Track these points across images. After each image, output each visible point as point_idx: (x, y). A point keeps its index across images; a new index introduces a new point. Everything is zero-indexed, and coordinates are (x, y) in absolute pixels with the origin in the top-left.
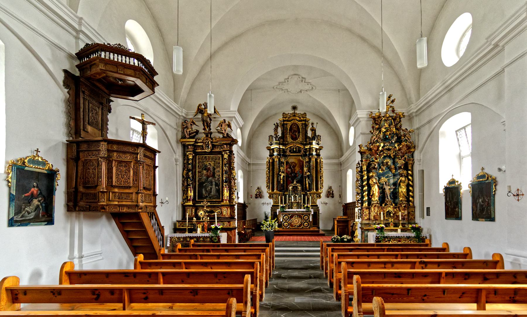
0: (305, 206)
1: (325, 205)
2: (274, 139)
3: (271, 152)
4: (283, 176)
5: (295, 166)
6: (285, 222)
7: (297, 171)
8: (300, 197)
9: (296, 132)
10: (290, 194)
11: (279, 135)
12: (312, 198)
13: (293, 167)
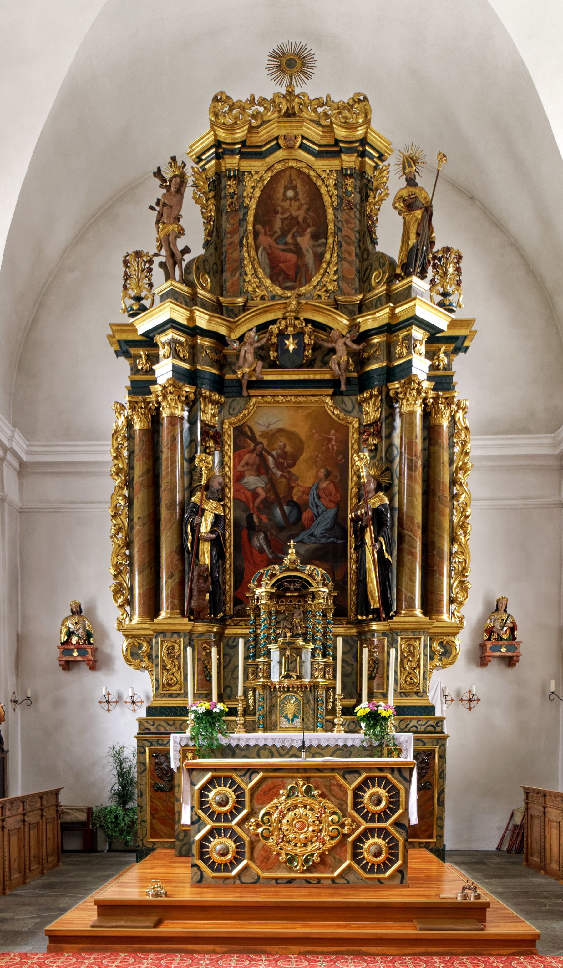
0: (363, 709)
1: (462, 709)
2: (158, 274)
3: (142, 363)
4: (218, 520)
5: (295, 459)
6: (211, 833)
7: (307, 492)
8: (324, 655)
9: (302, 232)
10: (256, 636)
11: (186, 250)
12: (402, 662)
13: (278, 465)
